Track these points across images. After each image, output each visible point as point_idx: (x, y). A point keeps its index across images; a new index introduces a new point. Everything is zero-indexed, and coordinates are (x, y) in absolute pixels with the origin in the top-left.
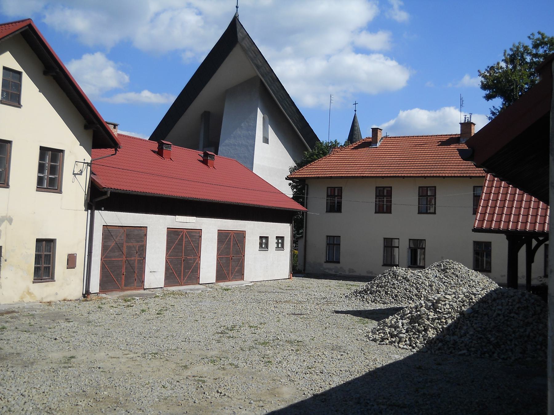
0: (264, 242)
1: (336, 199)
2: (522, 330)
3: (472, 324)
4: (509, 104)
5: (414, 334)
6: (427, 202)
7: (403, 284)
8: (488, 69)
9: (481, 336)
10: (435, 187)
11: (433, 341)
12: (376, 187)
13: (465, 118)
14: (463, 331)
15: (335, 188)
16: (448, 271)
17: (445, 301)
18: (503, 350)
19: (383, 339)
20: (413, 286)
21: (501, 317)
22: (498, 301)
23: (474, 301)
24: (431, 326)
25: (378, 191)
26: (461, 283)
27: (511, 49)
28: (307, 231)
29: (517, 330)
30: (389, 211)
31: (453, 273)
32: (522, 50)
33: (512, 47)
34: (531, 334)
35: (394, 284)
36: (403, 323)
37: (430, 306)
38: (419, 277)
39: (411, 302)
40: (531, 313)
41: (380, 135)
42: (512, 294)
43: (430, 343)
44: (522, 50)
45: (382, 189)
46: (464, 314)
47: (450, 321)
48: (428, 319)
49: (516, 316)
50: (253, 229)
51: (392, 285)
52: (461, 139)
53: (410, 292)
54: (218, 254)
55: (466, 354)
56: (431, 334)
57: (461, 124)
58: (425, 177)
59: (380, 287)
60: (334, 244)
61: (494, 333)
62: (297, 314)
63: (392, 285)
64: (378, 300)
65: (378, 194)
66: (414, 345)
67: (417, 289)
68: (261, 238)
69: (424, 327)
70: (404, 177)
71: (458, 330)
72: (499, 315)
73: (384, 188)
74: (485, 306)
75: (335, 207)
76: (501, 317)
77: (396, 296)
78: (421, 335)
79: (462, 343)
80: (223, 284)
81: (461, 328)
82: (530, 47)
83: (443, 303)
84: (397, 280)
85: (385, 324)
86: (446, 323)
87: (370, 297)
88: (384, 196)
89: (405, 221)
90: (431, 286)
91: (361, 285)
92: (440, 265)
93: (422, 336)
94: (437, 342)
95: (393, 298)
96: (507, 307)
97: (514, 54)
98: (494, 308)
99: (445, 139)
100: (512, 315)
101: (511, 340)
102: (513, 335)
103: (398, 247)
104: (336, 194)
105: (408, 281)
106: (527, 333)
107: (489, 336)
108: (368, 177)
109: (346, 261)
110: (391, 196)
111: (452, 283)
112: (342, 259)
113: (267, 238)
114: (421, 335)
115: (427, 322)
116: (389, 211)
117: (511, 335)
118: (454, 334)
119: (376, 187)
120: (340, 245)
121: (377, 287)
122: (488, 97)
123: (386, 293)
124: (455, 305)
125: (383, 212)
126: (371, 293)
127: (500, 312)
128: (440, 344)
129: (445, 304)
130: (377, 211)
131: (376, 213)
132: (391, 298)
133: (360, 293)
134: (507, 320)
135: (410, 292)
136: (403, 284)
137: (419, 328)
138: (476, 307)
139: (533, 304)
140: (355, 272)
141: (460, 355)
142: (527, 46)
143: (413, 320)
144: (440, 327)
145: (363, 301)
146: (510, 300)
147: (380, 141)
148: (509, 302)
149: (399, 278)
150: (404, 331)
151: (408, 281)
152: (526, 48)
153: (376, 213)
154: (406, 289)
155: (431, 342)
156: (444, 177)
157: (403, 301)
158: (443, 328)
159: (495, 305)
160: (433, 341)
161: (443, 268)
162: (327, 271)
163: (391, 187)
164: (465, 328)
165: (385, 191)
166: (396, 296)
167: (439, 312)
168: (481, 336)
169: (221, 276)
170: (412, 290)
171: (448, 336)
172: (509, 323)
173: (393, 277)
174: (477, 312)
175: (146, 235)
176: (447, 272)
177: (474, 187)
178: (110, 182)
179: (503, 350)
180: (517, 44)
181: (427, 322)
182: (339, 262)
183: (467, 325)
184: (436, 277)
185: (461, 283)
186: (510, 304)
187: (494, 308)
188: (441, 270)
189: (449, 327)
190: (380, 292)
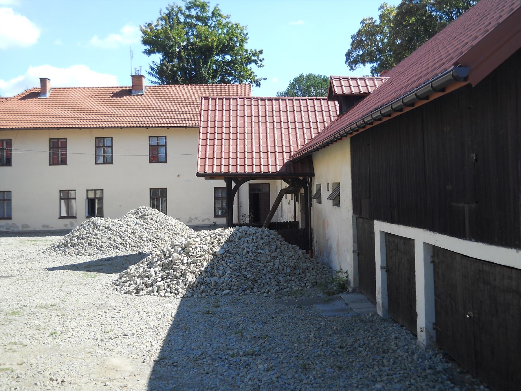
1: (60, 151)
2: (272, 264)
3: (227, 264)
4: (376, 52)
5: (172, 280)
6: (104, 152)
7: (107, 233)
8: (146, 26)
9: (239, 274)
10: (112, 138)
11: (194, 285)
12: (50, 139)
13: (136, 71)
14: (221, 272)
15: (3, 140)
16: (146, 217)
17: (195, 245)
18: (260, 285)
19: (138, 291)
20: (116, 235)
21: (250, 254)
22: (243, 239)
23: (222, 241)
24: (188, 271)
25: (52, 143)
26: (161, 227)
27: (167, 8)
29: (268, 264)
30: (64, 162)
31: (152, 219)
32: (176, 9)
33: (168, 7)
34: (280, 267)
35: (96, 235)
36: (156, 271)
37: (180, 251)
38: (120, 226)
39: (117, 250)
40: (273, 247)
41: (50, 85)
42: (254, 232)
43: (192, 288)
45: (56, 140)
46: (216, 255)
47: (205, 264)
48: (183, 264)
49: (263, 252)
51: (95, 235)
52: (133, 91)
53: (114, 241)
55: (231, 293)
56: (191, 278)
57: (132, 76)
58: (103, 128)
59: (82, 239)
60: (4, 200)
61: (248, 269)
62: (5, 277)
63: (95, 235)
64: (83, 252)
65: (52, 146)
66: (176, 292)
67: (120, 237)
69: (181, 272)
70: (80, 128)
71: (216, 271)
72: (248, 252)
73: (58, 139)
74: (233, 245)
76: (250, 254)
77: (101, 246)
78: (180, 281)
79: (223, 283)
81: (217, 269)
82: (184, 8)
83: (193, 247)
84: (99, 230)
85: (131, 277)
86: (202, 265)
87: (72, 250)
88: (58, 148)
89: (82, 172)
90: (133, 233)
91: (57, 240)
92: (137, 212)
93: (182, 282)
94: (199, 285)
95: (98, 249)
96: (253, 244)
97: (169, 13)
98: (242, 247)
99: (116, 91)
100: (259, 251)
101: (265, 275)
102: (265, 270)
103: (75, 199)
104: (60, 146)
105: (111, 230)
106: (277, 266)
107: (246, 273)
108: (42, 128)
109: (19, 215)
110: (66, 147)
111: (153, 228)
112: (14, 215)
114: (180, 281)
115: (184, 267)
116: (64, 162)
117: (263, 270)
118: (212, 275)
119: (50, 139)
120: (10, 200)
121: (78, 238)
122: (149, 53)
123: (90, 244)
124: (205, 247)
125: (58, 164)
126: (72, 246)
127: (248, 250)
128: (202, 287)
129: (196, 248)
130: (51, 163)
132: (96, 249)
133: (58, 247)
134: (256, 256)
135: (114, 241)
136: (107, 233)
137: (175, 273)
138: (226, 246)
139: (273, 239)
140: (29, 227)
141: (225, 295)
143: (164, 268)
144: (197, 270)
145: (65, 255)
146: (254, 238)
147: (49, 92)
148: (253, 239)
149: (101, 228)
150: (159, 279)
151: (111, 230)
152: (180, 10)
153: (50, 165)
154: (110, 239)
155: (193, 287)
156: (122, 128)
157: (109, 251)
158: (200, 271)
159: (242, 243)
160: (194, 285)
161: (140, 215)
163: (66, 139)
164: (221, 268)
165: (60, 143)
166: (101, 246)
167: (191, 256)
168: (239, 274)
170: (116, 239)
171: (207, 278)
172: (259, 259)
173: (94, 228)
174: (228, 252)
176: (145, 219)
177: (150, 137)
179: (260, 285)
180: (172, 4)
181: (184, 267)
182: (10, 218)
183: (223, 266)
184: (137, 224)
185: (161, 227)
186: (254, 241)
187: (242, 247)
188: (140, 217)
189: (206, 268)
190: (83, 244)
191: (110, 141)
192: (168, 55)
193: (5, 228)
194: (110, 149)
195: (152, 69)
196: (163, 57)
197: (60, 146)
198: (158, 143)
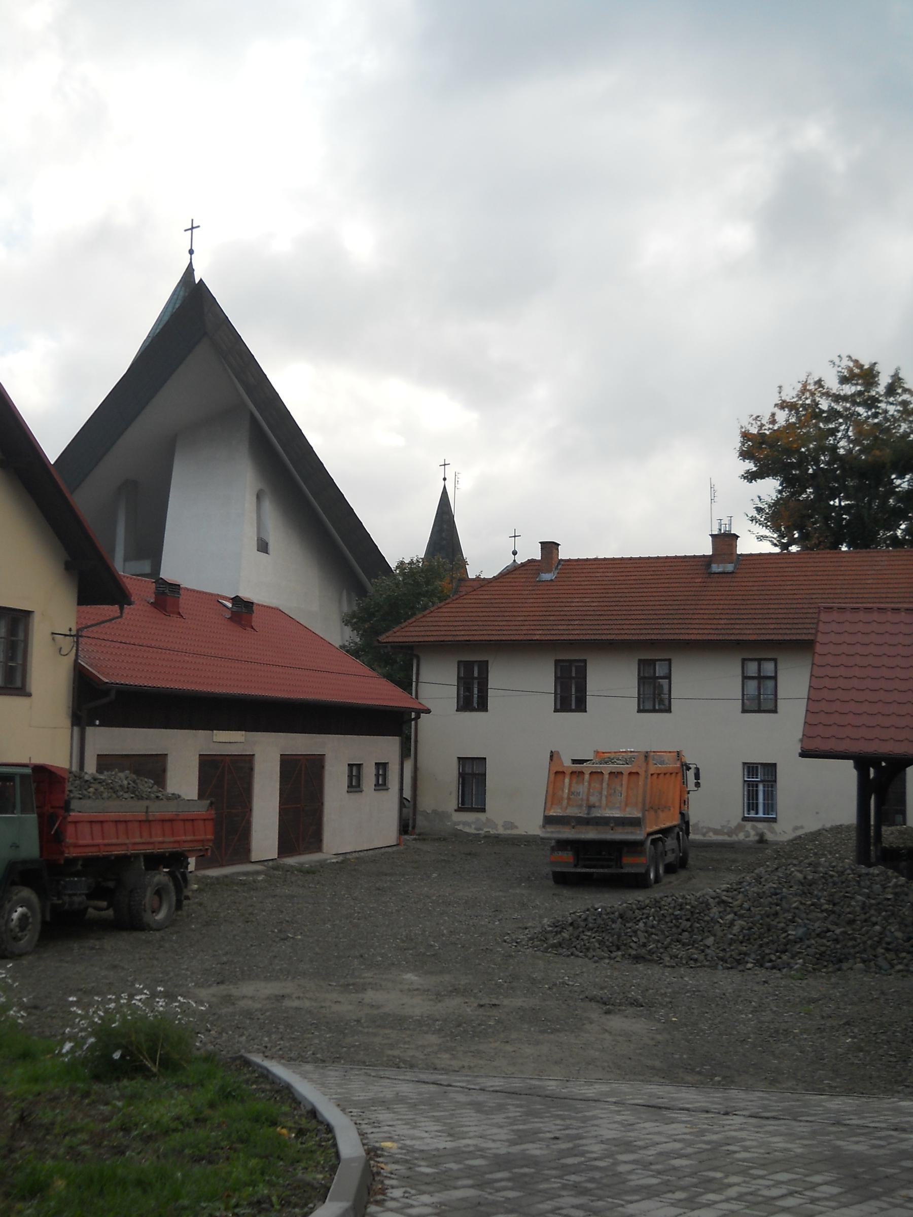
0: (355, 773)
28: (419, 749)
30: (483, 706)
44: (811, 387)
50: (338, 751)
54: (281, 803)
57: (711, 535)
68: (350, 766)
75: (473, 696)
80: (291, 861)
113: (359, 766)
122: (751, 477)
125: (473, 710)
131: (556, 711)
140: (516, 827)
142: (900, 379)
153: (556, 711)
162: (460, 827)
169: (287, 846)
175: (252, 769)
178: (118, 670)
182: (483, 810)
191: (667, 667)
192: (791, 483)
193: (473, 826)
194: (664, 682)
195: (759, 510)
196: (781, 485)
197: (574, 675)
198: (76, 827)
